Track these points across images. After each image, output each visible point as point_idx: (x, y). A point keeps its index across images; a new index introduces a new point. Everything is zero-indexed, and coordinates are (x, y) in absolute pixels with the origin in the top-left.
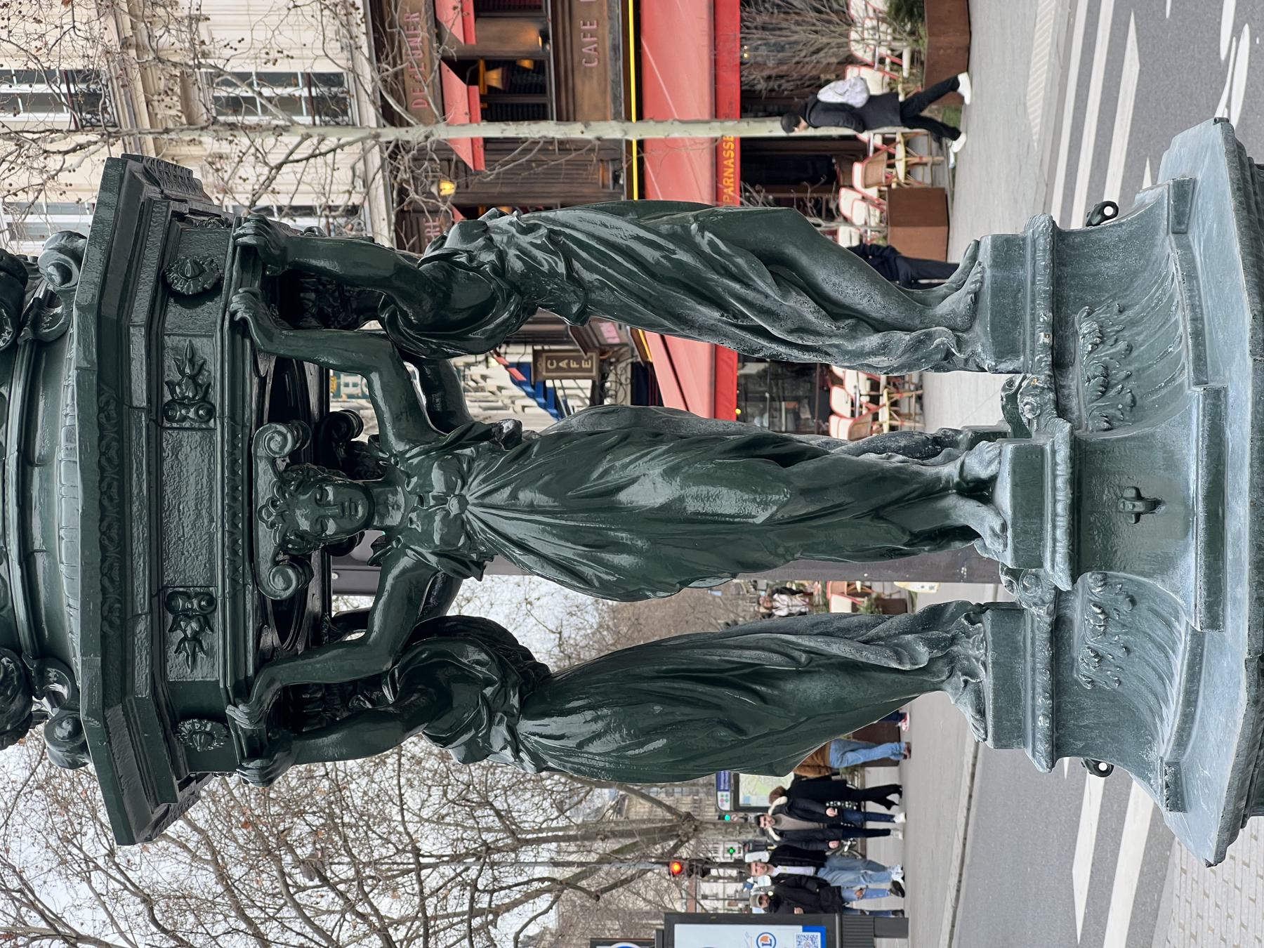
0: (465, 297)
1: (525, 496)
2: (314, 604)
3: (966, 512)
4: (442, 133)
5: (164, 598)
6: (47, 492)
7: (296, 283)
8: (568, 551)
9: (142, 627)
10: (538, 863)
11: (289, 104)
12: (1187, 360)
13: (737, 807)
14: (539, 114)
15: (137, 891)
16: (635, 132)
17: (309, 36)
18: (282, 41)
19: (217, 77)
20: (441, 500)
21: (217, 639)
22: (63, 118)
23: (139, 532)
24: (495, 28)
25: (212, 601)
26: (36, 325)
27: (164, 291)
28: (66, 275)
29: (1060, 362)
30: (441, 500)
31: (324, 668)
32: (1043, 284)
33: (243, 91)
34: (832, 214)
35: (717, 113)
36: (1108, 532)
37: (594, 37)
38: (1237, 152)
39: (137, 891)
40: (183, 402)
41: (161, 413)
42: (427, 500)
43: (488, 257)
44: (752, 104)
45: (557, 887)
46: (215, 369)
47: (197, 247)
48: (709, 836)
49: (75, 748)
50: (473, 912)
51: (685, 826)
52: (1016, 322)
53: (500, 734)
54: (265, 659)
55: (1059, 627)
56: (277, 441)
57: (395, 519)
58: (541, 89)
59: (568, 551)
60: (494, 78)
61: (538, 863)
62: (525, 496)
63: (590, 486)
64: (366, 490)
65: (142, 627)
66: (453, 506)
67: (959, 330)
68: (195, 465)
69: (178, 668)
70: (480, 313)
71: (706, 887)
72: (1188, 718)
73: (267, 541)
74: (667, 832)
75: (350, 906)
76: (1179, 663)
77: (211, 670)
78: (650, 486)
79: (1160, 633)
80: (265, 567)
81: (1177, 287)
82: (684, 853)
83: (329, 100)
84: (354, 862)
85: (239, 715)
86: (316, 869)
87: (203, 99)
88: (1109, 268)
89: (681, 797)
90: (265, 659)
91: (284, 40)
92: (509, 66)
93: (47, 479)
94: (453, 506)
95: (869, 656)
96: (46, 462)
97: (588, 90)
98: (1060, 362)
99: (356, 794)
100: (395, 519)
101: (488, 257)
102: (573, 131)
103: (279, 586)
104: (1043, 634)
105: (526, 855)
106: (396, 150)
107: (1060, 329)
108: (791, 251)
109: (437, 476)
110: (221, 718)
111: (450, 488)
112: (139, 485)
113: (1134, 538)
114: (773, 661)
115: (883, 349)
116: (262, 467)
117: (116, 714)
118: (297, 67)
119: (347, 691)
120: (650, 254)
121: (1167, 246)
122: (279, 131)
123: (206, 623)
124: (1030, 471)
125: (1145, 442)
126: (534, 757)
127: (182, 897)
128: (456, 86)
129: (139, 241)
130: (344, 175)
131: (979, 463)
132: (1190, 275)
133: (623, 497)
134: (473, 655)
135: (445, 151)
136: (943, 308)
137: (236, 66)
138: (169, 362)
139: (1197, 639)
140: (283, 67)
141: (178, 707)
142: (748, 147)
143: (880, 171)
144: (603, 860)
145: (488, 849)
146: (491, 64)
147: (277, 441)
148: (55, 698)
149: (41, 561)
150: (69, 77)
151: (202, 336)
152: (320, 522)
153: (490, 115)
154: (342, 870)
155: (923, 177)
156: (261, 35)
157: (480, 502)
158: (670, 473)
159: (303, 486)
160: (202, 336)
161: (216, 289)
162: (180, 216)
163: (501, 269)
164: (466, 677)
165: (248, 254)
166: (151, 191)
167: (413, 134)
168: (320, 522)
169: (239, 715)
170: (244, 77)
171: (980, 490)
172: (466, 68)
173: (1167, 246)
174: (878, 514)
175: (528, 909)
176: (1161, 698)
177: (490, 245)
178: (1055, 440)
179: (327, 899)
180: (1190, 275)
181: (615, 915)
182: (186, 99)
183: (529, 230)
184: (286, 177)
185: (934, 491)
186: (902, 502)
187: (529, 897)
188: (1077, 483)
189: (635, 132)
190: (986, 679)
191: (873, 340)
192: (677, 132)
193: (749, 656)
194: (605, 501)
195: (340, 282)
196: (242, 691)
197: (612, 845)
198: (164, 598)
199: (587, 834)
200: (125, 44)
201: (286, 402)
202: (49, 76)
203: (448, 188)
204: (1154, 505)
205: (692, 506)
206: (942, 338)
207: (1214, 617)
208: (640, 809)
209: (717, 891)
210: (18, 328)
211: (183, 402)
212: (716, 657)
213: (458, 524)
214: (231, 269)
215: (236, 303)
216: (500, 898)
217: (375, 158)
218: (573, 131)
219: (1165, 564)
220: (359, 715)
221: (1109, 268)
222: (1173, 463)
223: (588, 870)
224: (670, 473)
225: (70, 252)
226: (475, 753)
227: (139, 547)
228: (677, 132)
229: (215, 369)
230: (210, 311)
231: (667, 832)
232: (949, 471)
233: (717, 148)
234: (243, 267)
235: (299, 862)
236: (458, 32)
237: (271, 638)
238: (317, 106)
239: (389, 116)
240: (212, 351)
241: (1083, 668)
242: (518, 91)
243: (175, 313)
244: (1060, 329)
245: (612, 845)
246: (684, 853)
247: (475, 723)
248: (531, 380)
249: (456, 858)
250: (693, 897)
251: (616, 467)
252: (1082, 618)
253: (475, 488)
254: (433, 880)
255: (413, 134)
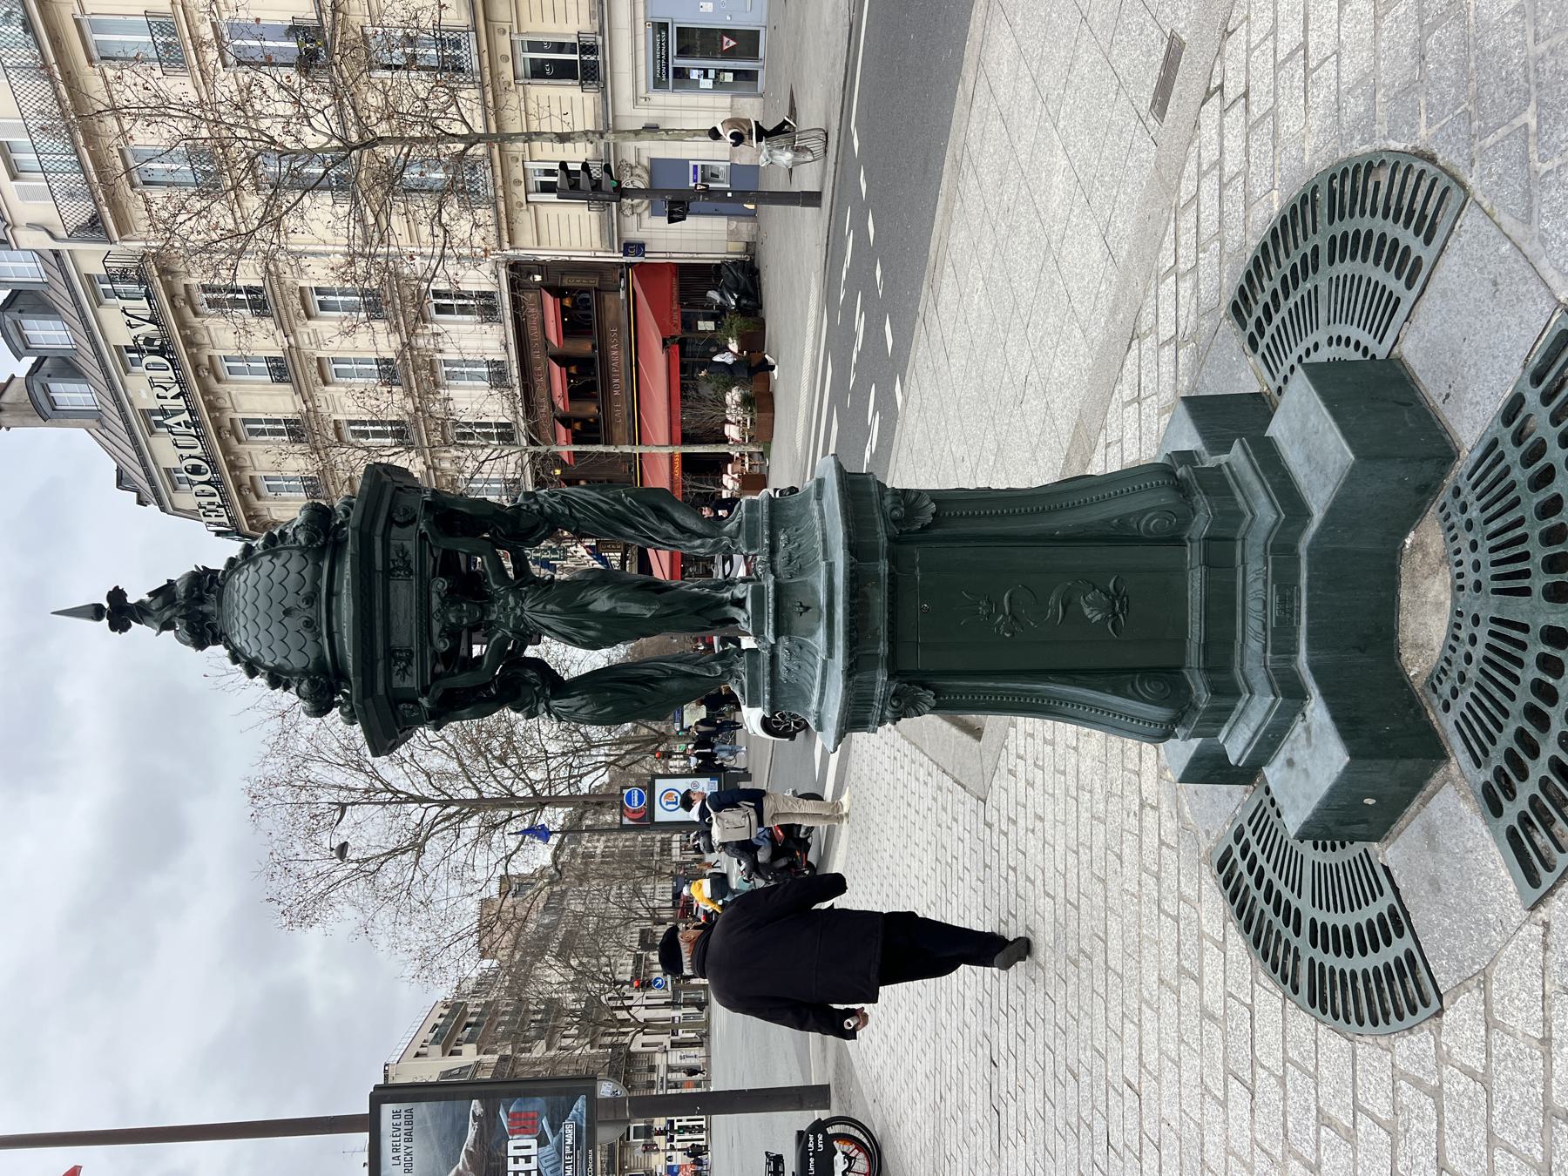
0: (525, 523)
1: (549, 607)
2: (463, 652)
3: (735, 612)
4: (554, 449)
5: (390, 652)
6: (339, 607)
7: (455, 517)
8: (568, 630)
9: (380, 665)
10: (600, 755)
11: (488, 436)
12: (820, 551)
13: (682, 729)
14: (596, 442)
15: (424, 771)
16: (637, 450)
17: (496, 407)
18: (485, 409)
19: (456, 424)
20: (513, 609)
21: (414, 669)
22: (389, 441)
23: (379, 623)
24: (577, 405)
25: (411, 653)
26: (335, 535)
27: (390, 521)
28: (347, 514)
29: (773, 550)
30: (513, 609)
31: (463, 680)
32: (766, 519)
33: (468, 430)
34: (721, 485)
35: (671, 443)
36: (789, 620)
37: (620, 411)
38: (839, 468)
39: (424, 771)
40: (398, 568)
41: (388, 573)
42: (507, 609)
43: (536, 507)
44: (687, 439)
45: (608, 765)
46: (413, 553)
47: (407, 500)
48: (672, 741)
49: (350, 719)
50: (571, 777)
51: (662, 737)
52: (756, 535)
53: (542, 706)
54: (436, 677)
55: (774, 658)
56: (441, 584)
57: (493, 617)
58: (598, 431)
59: (568, 630)
60: (577, 426)
61: (600, 755)
62: (549, 607)
63: (575, 603)
64: (481, 606)
65: (380, 665)
66: (518, 612)
67: (733, 537)
68: (403, 594)
69: (397, 682)
70: (533, 530)
71: (671, 763)
72: (822, 694)
73: (436, 627)
74: (654, 741)
75: (518, 776)
76: (818, 672)
77: (411, 683)
78: (602, 602)
79: (811, 660)
80: (435, 638)
81: (817, 521)
82: (661, 749)
83: (506, 434)
84: (519, 757)
85: (424, 701)
86: (502, 760)
87: (451, 433)
88: (792, 513)
89: (661, 727)
90: (436, 677)
91: (487, 408)
92: (584, 421)
93: (339, 601)
94: (518, 612)
95: (697, 671)
96: (339, 594)
97: (618, 432)
98: (773, 550)
99: (519, 729)
100: (493, 617)
101: (536, 507)
102: (611, 449)
103: (442, 646)
104: (767, 662)
105: (594, 752)
106: (534, 456)
107: (773, 538)
108: (664, 505)
109: (511, 599)
110: (417, 703)
111: (517, 604)
112: (379, 604)
113: (800, 622)
114: (658, 674)
115: (702, 546)
116: (434, 595)
117: (369, 702)
118: (491, 420)
119: (474, 690)
120: (604, 506)
121: (814, 505)
122: (483, 447)
123: (409, 663)
124: (758, 595)
125: (804, 583)
126: (557, 716)
127: (442, 773)
128: (562, 430)
129: (380, 497)
130: (512, 466)
131: (740, 591)
132: (822, 517)
133: (591, 607)
134: (530, 673)
135: (556, 456)
136: (727, 528)
137: (464, 419)
138: (392, 551)
139: (825, 662)
140: (484, 420)
141: (396, 699)
142: (685, 457)
143: (739, 467)
144: (628, 753)
145: (577, 750)
146: (577, 420)
147: (441, 584)
148: (345, 694)
149: (337, 636)
150: (392, 423)
151: (406, 539)
152: (460, 619)
153: (575, 442)
154: (513, 760)
155: (756, 470)
156: (476, 406)
157: (531, 611)
158: (610, 598)
159: (452, 604)
160: (406, 539)
161: (413, 521)
162: (400, 489)
163: (541, 511)
164: (527, 683)
165: (428, 506)
166: (386, 478)
167: (542, 449)
168: (460, 619)
169: (424, 701)
170: (468, 424)
171: (740, 603)
172: (566, 421)
173: (814, 505)
174: (698, 613)
175: (594, 775)
176: (813, 686)
177: (536, 502)
178: (769, 583)
179: (507, 773)
180: (822, 517)
181: (634, 775)
182: (443, 432)
183: (553, 495)
184: (486, 467)
185: (722, 603)
186: (709, 608)
187: (595, 769)
188: (777, 600)
189: (637, 450)
190: (745, 680)
191: (698, 542)
192: (655, 450)
193: (647, 672)
194: (583, 609)
195: (471, 517)
196: (425, 691)
197: (631, 747)
198: (390, 652)
199: (621, 742)
200: (417, 410)
201: (448, 565)
202: (382, 423)
203: (558, 472)
204: (807, 609)
205: (620, 611)
206: (726, 541)
207: (830, 654)
208: (644, 731)
209: (676, 764)
210: (327, 537)
211: (398, 568)
212: (633, 672)
213: (520, 619)
214: (420, 512)
215: (422, 526)
216: (582, 770)
217: (526, 458)
218: (611, 449)
219: (812, 633)
220: (481, 700)
221: (792, 513)
222: (815, 592)
223: (621, 757)
224: (610, 598)
225: (349, 504)
226: (530, 715)
227: (379, 631)
228: (655, 450)
229: (413, 553)
230: (411, 529)
231: (654, 741)
232: (728, 595)
233: (672, 456)
234: (426, 510)
235: (494, 758)
236: (561, 406)
237: (440, 668)
238: (500, 436)
239: (532, 442)
240: (411, 546)
241: (783, 674)
242: (586, 432)
243: (395, 530)
244: (773, 538)
245: (631, 747)
246: (661, 749)
247: (531, 702)
248: (594, 552)
249: (563, 754)
250: (666, 767)
251: (590, 595)
252: (782, 654)
253: (528, 604)
254: (554, 764)
255: (542, 449)
